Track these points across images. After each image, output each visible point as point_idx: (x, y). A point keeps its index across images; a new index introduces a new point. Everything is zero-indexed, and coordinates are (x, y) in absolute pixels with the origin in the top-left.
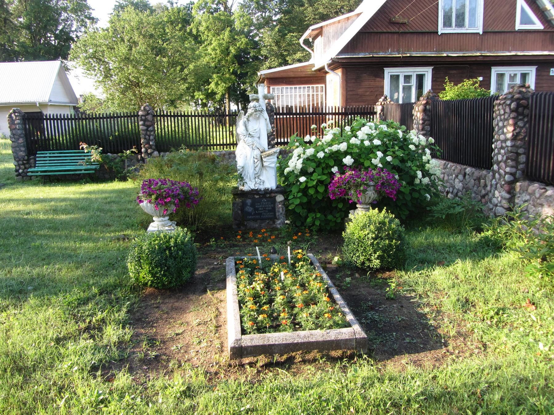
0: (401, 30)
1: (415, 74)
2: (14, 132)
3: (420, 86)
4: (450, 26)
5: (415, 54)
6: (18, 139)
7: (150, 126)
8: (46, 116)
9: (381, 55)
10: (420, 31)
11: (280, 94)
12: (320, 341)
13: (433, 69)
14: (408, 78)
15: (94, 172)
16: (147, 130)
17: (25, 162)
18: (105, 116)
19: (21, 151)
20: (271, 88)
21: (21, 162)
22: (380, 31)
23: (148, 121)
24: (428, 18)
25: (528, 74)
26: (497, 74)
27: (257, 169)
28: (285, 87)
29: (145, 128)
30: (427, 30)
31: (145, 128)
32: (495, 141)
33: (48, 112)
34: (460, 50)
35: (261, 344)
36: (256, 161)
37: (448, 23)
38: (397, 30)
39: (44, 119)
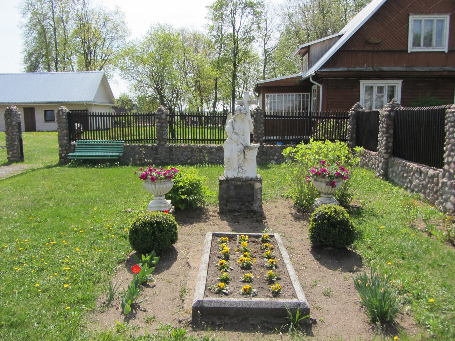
0: (376, 49)
1: (387, 85)
2: (60, 125)
3: (391, 96)
4: (419, 45)
5: (386, 69)
6: (63, 130)
7: (164, 123)
8: (90, 113)
9: (357, 69)
10: (392, 49)
11: (273, 100)
12: (268, 308)
13: (403, 82)
14: (380, 89)
15: (117, 157)
16: (161, 126)
17: (67, 148)
18: (108, 114)
19: (65, 140)
20: (265, 95)
21: (64, 148)
22: (357, 49)
23: (162, 119)
24: (399, 39)
25: (395, 86)
26: (366, 87)
27: (240, 161)
28: (277, 94)
29: (159, 124)
30: (398, 49)
31: (159, 124)
32: (446, 145)
33: (94, 110)
34: (428, 66)
35: (219, 306)
36: (239, 154)
37: (416, 43)
38: (372, 49)
39: (89, 116)
